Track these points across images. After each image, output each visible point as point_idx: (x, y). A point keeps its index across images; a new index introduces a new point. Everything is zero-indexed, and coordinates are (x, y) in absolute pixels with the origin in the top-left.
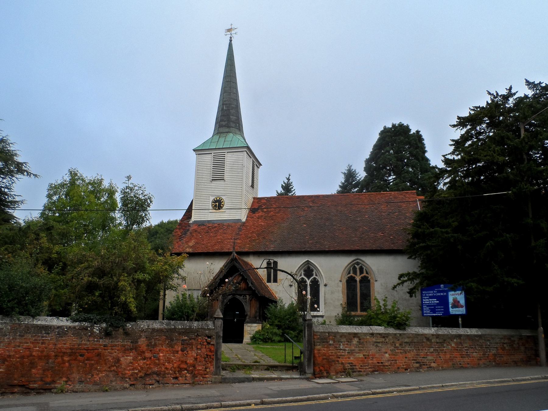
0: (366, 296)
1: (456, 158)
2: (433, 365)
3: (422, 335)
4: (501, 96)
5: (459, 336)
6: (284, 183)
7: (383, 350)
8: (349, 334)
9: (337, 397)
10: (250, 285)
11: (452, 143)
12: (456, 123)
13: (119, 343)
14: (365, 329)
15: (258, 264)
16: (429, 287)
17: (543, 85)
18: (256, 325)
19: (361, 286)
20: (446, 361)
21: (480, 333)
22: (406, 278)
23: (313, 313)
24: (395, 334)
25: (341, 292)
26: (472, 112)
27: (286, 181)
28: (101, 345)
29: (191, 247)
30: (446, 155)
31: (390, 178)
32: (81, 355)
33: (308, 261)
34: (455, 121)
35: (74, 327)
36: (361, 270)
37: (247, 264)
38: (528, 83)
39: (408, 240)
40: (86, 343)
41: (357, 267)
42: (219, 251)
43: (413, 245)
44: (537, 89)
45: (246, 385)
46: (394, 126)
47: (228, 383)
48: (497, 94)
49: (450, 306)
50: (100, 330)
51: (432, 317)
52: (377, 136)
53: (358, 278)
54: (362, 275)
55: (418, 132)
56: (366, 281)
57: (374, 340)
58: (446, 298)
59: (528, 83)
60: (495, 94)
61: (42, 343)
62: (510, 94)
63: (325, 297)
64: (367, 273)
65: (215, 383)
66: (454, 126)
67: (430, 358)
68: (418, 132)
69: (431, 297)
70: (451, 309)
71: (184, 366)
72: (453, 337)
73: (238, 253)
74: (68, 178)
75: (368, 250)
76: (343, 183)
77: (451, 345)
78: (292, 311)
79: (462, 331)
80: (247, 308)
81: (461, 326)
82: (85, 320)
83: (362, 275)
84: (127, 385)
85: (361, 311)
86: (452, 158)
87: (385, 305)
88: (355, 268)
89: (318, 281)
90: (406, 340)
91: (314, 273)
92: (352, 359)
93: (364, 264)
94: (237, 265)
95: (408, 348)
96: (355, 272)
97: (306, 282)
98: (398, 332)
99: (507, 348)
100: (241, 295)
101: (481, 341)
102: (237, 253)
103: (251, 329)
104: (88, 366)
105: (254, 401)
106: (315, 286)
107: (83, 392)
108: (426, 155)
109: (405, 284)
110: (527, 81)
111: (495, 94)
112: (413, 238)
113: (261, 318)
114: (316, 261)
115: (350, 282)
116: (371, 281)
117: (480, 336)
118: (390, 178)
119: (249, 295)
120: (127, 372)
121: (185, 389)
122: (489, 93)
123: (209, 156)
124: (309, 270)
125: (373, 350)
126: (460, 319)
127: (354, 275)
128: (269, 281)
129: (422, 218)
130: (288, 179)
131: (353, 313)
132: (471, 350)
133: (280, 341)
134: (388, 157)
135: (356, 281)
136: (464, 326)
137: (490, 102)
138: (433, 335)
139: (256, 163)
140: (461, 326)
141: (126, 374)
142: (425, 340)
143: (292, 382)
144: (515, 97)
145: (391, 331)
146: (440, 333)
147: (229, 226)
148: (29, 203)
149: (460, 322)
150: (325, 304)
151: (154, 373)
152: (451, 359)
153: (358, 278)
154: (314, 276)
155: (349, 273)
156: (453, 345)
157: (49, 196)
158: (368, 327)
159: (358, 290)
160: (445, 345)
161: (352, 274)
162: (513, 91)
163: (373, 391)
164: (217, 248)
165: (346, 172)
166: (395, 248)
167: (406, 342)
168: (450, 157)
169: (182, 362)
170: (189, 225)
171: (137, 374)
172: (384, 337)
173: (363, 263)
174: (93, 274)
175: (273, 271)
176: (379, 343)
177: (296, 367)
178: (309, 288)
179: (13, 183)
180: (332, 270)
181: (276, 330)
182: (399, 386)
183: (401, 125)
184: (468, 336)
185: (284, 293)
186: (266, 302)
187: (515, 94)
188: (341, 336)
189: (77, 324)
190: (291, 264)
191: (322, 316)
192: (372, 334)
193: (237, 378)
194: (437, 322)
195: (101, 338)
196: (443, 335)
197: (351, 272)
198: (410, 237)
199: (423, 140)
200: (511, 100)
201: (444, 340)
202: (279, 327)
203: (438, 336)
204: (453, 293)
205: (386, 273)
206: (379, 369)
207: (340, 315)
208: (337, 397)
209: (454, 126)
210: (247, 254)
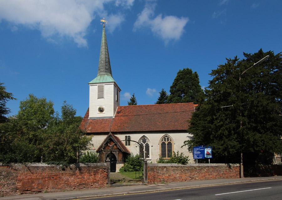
0: (170, 150)
1: (210, 90)
2: (197, 178)
3: (193, 166)
4: (232, 60)
5: (208, 167)
6: (131, 98)
7: (177, 173)
8: (163, 167)
9: (157, 191)
10: (118, 147)
11: (209, 82)
12: (211, 73)
13: (68, 172)
14: (169, 165)
15: (122, 137)
16: (197, 147)
17: (252, 55)
18: (121, 164)
19: (168, 146)
20: (202, 177)
21: (217, 165)
22: (187, 143)
23: (147, 159)
24: (182, 166)
25: (159, 149)
26: (219, 68)
27: (132, 97)
28: (60, 173)
29: (90, 130)
30: (206, 88)
31: (182, 95)
32: (52, 178)
33: (144, 136)
34: (211, 72)
35: (49, 167)
36: (168, 139)
37: (116, 137)
38: (244, 54)
39: (189, 126)
40: (54, 173)
41: (166, 138)
42: (103, 132)
43: (190, 128)
44: (248, 57)
45: (120, 187)
46: (184, 70)
47: (113, 187)
48: (230, 60)
49: (205, 154)
50: (59, 167)
51: (198, 159)
52: (176, 75)
53: (166, 143)
54: (168, 142)
55: (196, 73)
56: (170, 144)
57: (173, 169)
58: (204, 151)
59: (244, 54)
60: (229, 59)
61: (36, 173)
62: (236, 59)
63: (152, 151)
64: (171, 141)
65: (108, 187)
66: (210, 74)
67: (195, 175)
68: (196, 73)
69: (197, 151)
70: (206, 156)
71: (95, 181)
72: (205, 167)
73: (112, 133)
74: (29, 98)
75: (171, 130)
76: (159, 98)
77: (204, 170)
78: (138, 158)
79: (209, 165)
80: (117, 157)
81: (209, 163)
82: (53, 164)
83: (168, 142)
84: (72, 189)
85: (168, 157)
86: (208, 90)
87: (178, 155)
88: (164, 138)
89: (148, 144)
90: (186, 169)
91: (147, 141)
92: (163, 176)
93: (169, 137)
94: (112, 138)
95: (187, 172)
96: (165, 140)
97: (143, 145)
98: (183, 165)
99: (228, 171)
100: (114, 151)
101: (217, 168)
102: (112, 132)
103: (119, 166)
104: (56, 182)
105: (125, 193)
106: (147, 147)
107: (55, 192)
108: (200, 84)
109: (187, 145)
110: (244, 53)
111: (229, 59)
112: (191, 125)
113: (124, 162)
114: (146, 135)
115: (163, 145)
116: (172, 144)
117: (217, 167)
118: (182, 95)
119: (118, 151)
120: (72, 184)
121: (96, 190)
122: (227, 59)
123: (97, 86)
124: (144, 139)
125: (172, 173)
126: (209, 160)
127: (165, 142)
128: (126, 145)
129: (195, 116)
130: (133, 96)
131: (164, 158)
132: (213, 172)
133: (132, 171)
134: (181, 85)
135: (166, 144)
136: (211, 162)
137: (227, 63)
138: (197, 166)
139: (118, 89)
140: (209, 163)
141: (72, 184)
142: (194, 169)
143: (139, 186)
144: (238, 61)
145: (180, 165)
146: (200, 166)
147: (107, 120)
148: (13, 110)
149: (209, 161)
150: (152, 154)
151: (84, 184)
152: (204, 176)
153: (166, 143)
154: (147, 142)
155: (163, 141)
156: (205, 170)
157: (21, 107)
158: (170, 164)
159: (166, 147)
160: (202, 170)
161: (163, 141)
162: (237, 58)
163: (172, 188)
164: (102, 131)
165: (161, 92)
166: (183, 129)
167: (186, 170)
168: (208, 89)
169: (94, 179)
170: (88, 120)
171: (76, 184)
172: (177, 168)
173: (169, 136)
174: (55, 144)
175: (128, 140)
176: (175, 170)
177: (140, 179)
178: (144, 149)
179: (5, 103)
180: (155, 140)
181: (130, 166)
182: (182, 186)
183: (188, 69)
184: (212, 166)
185: (134, 150)
186: (126, 155)
187: (238, 59)
188: (159, 168)
189: (49, 165)
190: (136, 137)
191: (151, 160)
192: (172, 167)
193: (117, 185)
194: (200, 161)
195: (60, 171)
196: (201, 166)
197: (164, 140)
198: (190, 124)
199: (198, 76)
200: (236, 62)
201: (201, 168)
202: (132, 165)
203: (199, 167)
204: (207, 149)
205: (180, 141)
206: (174, 180)
207: (159, 159)
208: (157, 191)
209: (210, 74)
210: (117, 133)
